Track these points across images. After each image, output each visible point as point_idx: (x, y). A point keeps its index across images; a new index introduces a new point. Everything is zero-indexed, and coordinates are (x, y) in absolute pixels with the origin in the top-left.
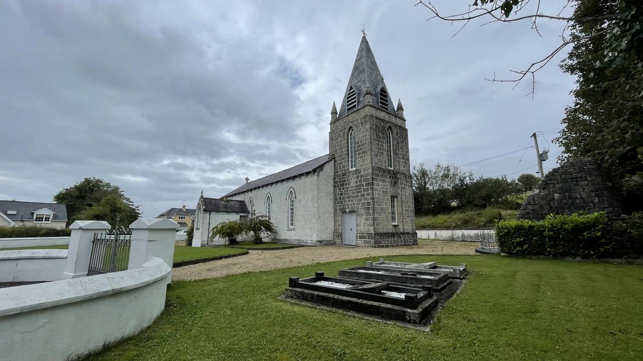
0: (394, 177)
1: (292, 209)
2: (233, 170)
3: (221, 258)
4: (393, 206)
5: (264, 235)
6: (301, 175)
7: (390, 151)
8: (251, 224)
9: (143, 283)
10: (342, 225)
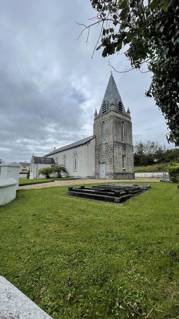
0: (124, 146)
1: (76, 162)
2: (51, 145)
3: (41, 183)
4: (123, 160)
5: (63, 174)
6: (80, 145)
7: (123, 133)
8: (56, 169)
9: (6, 185)
10: (99, 169)
